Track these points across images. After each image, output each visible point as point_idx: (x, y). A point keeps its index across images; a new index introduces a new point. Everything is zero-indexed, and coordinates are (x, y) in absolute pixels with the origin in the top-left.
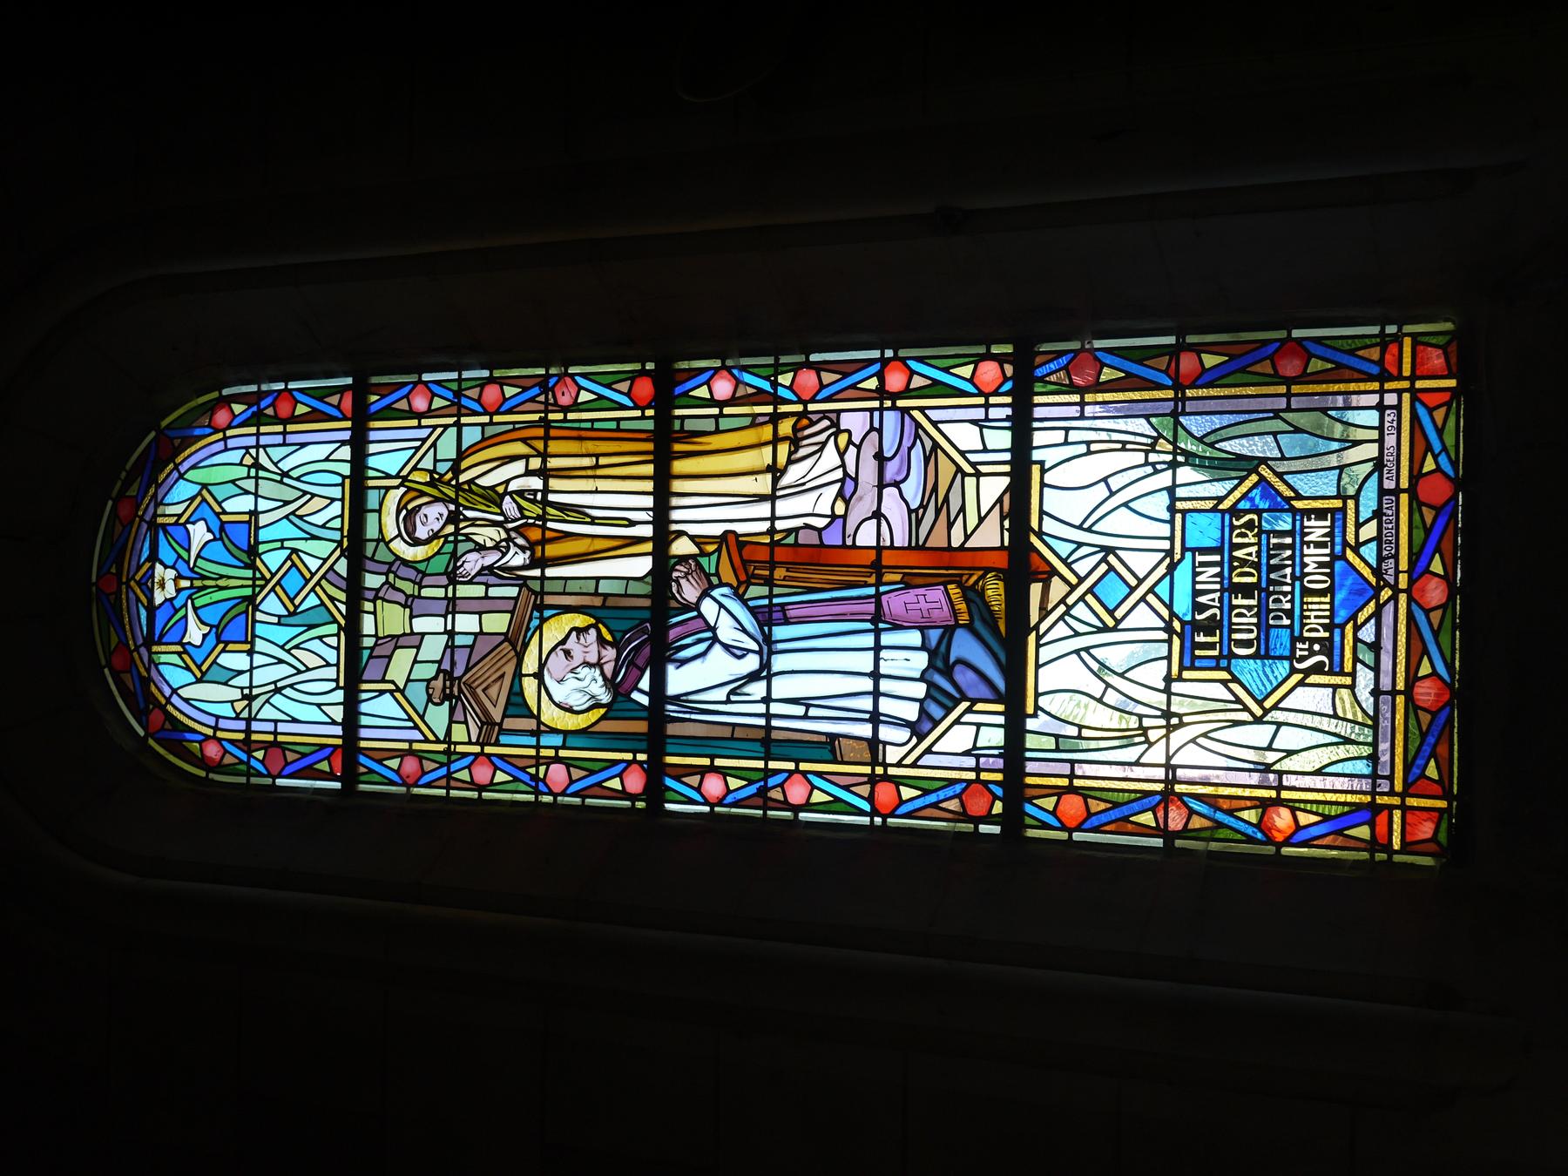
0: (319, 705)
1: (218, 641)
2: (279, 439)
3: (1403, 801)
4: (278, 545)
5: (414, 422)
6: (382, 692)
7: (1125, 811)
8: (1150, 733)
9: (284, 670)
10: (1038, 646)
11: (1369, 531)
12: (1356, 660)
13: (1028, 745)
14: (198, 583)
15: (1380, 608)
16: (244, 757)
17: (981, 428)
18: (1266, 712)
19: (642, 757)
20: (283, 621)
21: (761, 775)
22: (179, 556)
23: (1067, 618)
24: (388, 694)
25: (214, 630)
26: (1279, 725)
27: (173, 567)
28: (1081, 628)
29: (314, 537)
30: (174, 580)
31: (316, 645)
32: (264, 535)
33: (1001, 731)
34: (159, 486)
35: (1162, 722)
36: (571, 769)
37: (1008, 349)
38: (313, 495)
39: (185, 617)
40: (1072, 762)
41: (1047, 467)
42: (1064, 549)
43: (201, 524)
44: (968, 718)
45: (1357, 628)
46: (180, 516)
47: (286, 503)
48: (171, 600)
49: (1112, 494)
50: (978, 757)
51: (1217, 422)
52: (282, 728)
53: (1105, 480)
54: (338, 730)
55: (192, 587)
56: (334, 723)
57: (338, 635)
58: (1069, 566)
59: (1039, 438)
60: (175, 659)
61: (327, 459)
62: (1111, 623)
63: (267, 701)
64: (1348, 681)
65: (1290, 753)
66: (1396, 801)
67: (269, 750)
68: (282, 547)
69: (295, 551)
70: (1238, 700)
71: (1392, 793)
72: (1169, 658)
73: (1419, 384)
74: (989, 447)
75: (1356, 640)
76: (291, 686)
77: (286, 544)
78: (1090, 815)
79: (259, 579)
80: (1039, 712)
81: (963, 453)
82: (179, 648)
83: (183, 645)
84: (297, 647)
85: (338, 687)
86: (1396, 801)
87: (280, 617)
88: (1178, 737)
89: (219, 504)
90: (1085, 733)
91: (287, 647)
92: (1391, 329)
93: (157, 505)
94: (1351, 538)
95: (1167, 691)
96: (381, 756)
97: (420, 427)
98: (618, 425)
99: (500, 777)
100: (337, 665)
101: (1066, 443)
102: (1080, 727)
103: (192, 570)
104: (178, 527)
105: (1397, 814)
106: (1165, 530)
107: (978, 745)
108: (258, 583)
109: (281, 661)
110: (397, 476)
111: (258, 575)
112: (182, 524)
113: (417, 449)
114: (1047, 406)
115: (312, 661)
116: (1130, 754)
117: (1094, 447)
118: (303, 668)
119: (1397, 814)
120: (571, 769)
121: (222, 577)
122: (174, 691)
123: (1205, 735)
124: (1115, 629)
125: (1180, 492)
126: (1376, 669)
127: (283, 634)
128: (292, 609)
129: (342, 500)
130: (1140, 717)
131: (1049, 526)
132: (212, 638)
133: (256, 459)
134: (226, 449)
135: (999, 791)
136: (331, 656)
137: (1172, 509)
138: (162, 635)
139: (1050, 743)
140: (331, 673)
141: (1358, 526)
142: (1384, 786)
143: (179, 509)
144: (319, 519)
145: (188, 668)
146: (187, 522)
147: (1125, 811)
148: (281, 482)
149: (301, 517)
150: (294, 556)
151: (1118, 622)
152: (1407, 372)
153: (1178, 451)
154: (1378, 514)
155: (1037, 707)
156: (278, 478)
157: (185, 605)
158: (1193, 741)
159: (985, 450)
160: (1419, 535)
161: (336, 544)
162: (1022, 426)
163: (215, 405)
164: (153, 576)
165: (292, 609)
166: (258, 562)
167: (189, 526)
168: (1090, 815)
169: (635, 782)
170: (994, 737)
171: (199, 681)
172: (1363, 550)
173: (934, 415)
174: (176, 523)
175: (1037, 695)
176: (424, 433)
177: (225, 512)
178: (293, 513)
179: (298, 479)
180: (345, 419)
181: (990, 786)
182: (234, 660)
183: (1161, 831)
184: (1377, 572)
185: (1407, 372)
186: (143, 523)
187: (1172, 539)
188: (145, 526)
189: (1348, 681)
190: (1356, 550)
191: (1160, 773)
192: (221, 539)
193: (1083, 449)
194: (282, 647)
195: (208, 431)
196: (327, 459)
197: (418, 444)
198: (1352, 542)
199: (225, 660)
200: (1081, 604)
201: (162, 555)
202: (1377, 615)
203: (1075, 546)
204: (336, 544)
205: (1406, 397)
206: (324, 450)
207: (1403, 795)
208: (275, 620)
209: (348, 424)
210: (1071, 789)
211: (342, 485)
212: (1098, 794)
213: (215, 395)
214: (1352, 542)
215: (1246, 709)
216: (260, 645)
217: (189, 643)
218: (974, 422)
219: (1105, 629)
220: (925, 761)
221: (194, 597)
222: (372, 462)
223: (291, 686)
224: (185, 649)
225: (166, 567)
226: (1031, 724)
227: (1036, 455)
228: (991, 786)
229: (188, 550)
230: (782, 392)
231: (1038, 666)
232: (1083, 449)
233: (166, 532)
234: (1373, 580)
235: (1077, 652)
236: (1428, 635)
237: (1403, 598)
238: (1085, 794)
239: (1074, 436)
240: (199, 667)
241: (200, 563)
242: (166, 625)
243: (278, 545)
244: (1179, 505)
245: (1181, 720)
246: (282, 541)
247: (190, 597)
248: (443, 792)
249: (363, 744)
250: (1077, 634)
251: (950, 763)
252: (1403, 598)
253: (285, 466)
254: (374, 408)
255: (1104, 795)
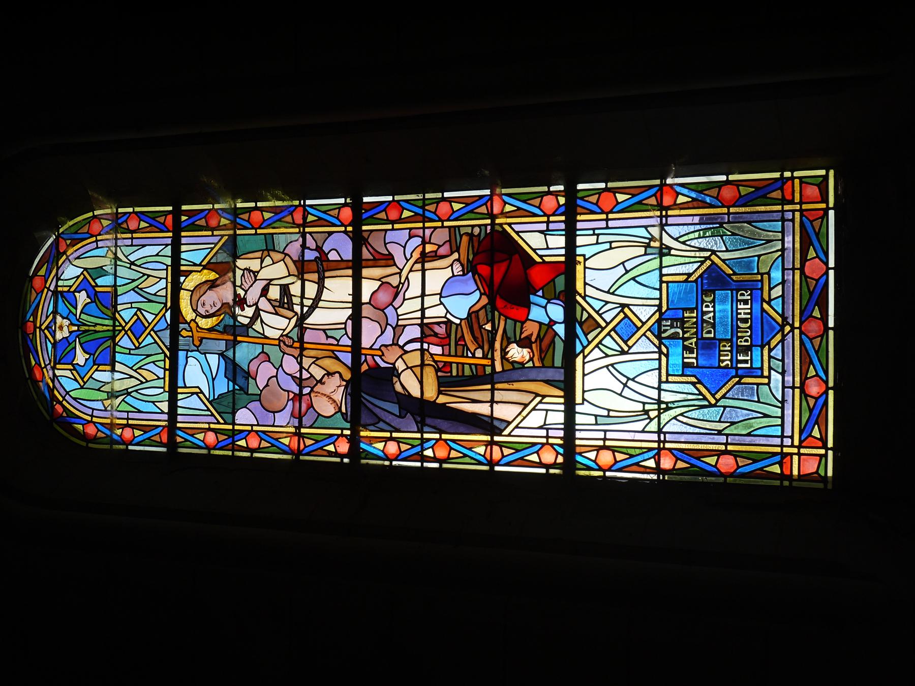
0: (153, 402)
1: (94, 364)
2: (129, 242)
3: (799, 451)
4: (129, 306)
5: (210, 233)
6: (193, 394)
7: (639, 458)
8: (651, 413)
9: (134, 382)
10: (584, 363)
11: (777, 292)
12: (770, 368)
13: (178, 420)
14: (83, 328)
15: (784, 336)
16: (108, 432)
17: (545, 235)
18: (717, 401)
19: (348, 432)
20: (132, 352)
21: (419, 442)
22: (71, 311)
23: (600, 346)
24: (195, 395)
25: (92, 356)
26: (725, 407)
27: (66, 318)
28: (610, 352)
29: (150, 301)
30: (68, 327)
31: (151, 367)
32: (120, 300)
33: (562, 414)
34: (58, 268)
35: (656, 407)
36: (616, 453)
37: (561, 188)
38: (149, 276)
39: (75, 348)
40: (605, 431)
41: (587, 257)
42: (597, 305)
43: (84, 293)
44: (540, 406)
45: (770, 350)
46: (71, 287)
47: (134, 281)
48: (66, 338)
49: (627, 272)
50: (548, 429)
51: (685, 229)
52: (131, 415)
53: (623, 263)
54: (165, 417)
55: (78, 330)
56: (163, 412)
57: (164, 361)
58: (600, 315)
59: (580, 241)
60: (68, 374)
61: (157, 255)
62: (626, 349)
63: (123, 400)
64: (766, 381)
65: (732, 423)
66: (795, 450)
67: (600, 451)
68: (132, 308)
69: (139, 309)
70: (701, 393)
71: (792, 446)
72: (660, 369)
73: (804, 207)
74: (550, 247)
75: (770, 357)
76: (136, 391)
77: (134, 305)
78: (616, 462)
79: (118, 326)
80: (585, 402)
81: (534, 250)
82: (70, 367)
83: (73, 365)
84: (140, 368)
85: (165, 391)
86: (795, 450)
87: (130, 349)
88: (665, 417)
89: (94, 280)
90: (612, 414)
91: (134, 368)
92: (787, 174)
93: (58, 279)
94: (766, 297)
95: (659, 389)
96: (193, 432)
97: (213, 235)
98: (130, 352)
99: (264, 444)
100: (164, 378)
101: (597, 243)
102: (609, 410)
103: (78, 320)
104: (70, 293)
105: (796, 458)
106: (656, 294)
107: (547, 423)
108: (117, 328)
109: (131, 377)
110: (200, 265)
111: (117, 324)
112: (71, 292)
113: (212, 249)
114: (584, 222)
115: (149, 376)
116: (639, 426)
117: (614, 245)
118: (144, 381)
119: (796, 458)
120: (616, 453)
121: (97, 324)
122: (68, 393)
123: (682, 414)
124: (627, 353)
125: (665, 271)
126: (783, 374)
127: (131, 360)
128: (137, 345)
129: (166, 278)
130: (644, 403)
131: (590, 291)
132: (91, 361)
133: (115, 254)
134: (97, 248)
135: (561, 450)
136: (160, 373)
137: (661, 282)
138: (60, 360)
139: (592, 420)
140: (160, 383)
141: (770, 289)
142: (788, 442)
143: (70, 283)
144: (152, 290)
145: (76, 380)
146: (75, 291)
147: (639, 458)
148: (130, 268)
149: (141, 289)
150: (138, 313)
151: (630, 348)
152: (797, 199)
153: (663, 246)
154: (783, 282)
155: (584, 400)
156: (128, 266)
157: (75, 341)
158: (675, 418)
159: (548, 248)
160: (806, 296)
161: (163, 305)
162: (571, 235)
163: (91, 220)
164: (55, 323)
165: (137, 345)
166: (117, 315)
167: (77, 294)
168: (616, 462)
169: (344, 447)
170: (559, 418)
171: (82, 388)
172: (772, 303)
173: (517, 228)
174: (69, 291)
175: (584, 392)
176: (215, 240)
177: (97, 286)
178: (137, 287)
179: (139, 266)
180: (168, 231)
181: (448, 442)
182: (103, 376)
183: (658, 470)
184: (782, 316)
185: (797, 199)
186: (49, 292)
187: (660, 299)
188: (50, 293)
189: (766, 381)
190: (769, 303)
191: (655, 437)
192: (95, 302)
193: (607, 246)
194: (131, 368)
195: (88, 235)
196: (157, 255)
197: (213, 246)
198: (767, 299)
199: (97, 375)
200: (608, 337)
201: (59, 311)
202: (782, 341)
203: (604, 303)
204: (163, 305)
205: (797, 214)
206: (156, 250)
207: (799, 447)
208: (128, 351)
209: (170, 234)
210: (605, 447)
211: (167, 270)
212: (309, 436)
213: (91, 214)
214: (767, 299)
215: (705, 398)
216: (118, 367)
217: (77, 364)
218: (541, 232)
219: (623, 352)
220: (515, 432)
221: (80, 337)
222: (183, 256)
223: (136, 391)
224: (75, 368)
225: (63, 318)
226: (578, 408)
227: (579, 251)
228: (555, 446)
229: (76, 309)
230: (428, 214)
231: (584, 375)
232: (607, 246)
233: (62, 296)
234: (779, 319)
235: (607, 366)
236: (812, 353)
237: (797, 332)
238: (613, 449)
239: (602, 239)
240: (82, 379)
241: (83, 316)
242: (62, 353)
243: (129, 306)
244: (665, 279)
245: (667, 405)
246: (131, 303)
247: (77, 336)
248: (230, 453)
249: (179, 425)
250: (607, 356)
251: (675, 439)
252: (797, 332)
253: (132, 258)
254: (183, 225)
255: (312, 437)
